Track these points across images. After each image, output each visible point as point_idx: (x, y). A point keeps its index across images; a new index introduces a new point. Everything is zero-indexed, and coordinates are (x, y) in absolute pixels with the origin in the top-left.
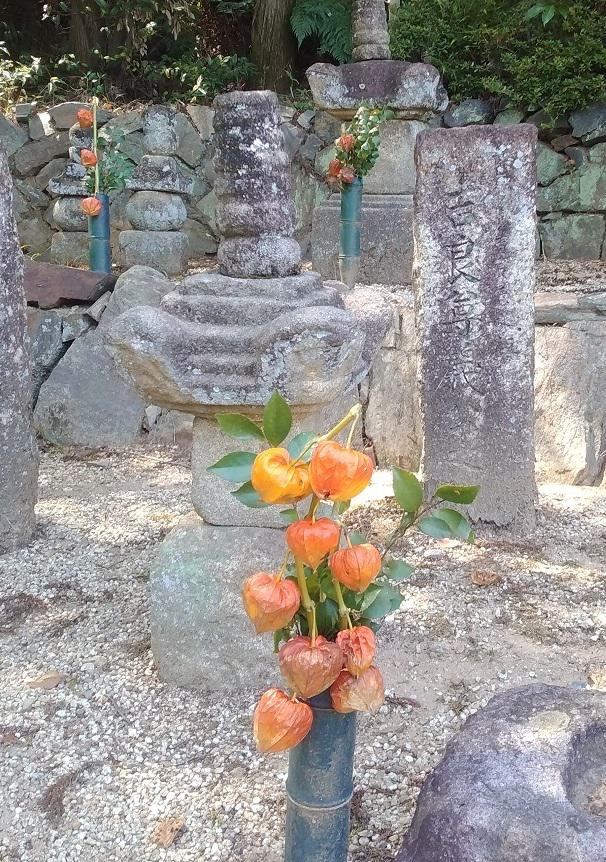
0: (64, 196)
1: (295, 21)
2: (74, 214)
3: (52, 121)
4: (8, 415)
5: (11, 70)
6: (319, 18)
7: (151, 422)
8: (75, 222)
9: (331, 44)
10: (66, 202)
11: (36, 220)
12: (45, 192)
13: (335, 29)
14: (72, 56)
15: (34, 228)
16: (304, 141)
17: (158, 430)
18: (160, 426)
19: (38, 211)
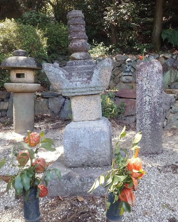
0: (124, 76)
1: (162, 35)
2: (127, 79)
3: (116, 59)
4: (161, 123)
5: (105, 48)
6: (168, 35)
7: (165, 126)
8: (127, 81)
9: (171, 40)
10: (125, 77)
11: (112, 81)
12: (114, 75)
13: (172, 37)
14: (114, 45)
15: (112, 83)
16: (175, 62)
17: (167, 127)
18: (167, 127)
19: (112, 79)
